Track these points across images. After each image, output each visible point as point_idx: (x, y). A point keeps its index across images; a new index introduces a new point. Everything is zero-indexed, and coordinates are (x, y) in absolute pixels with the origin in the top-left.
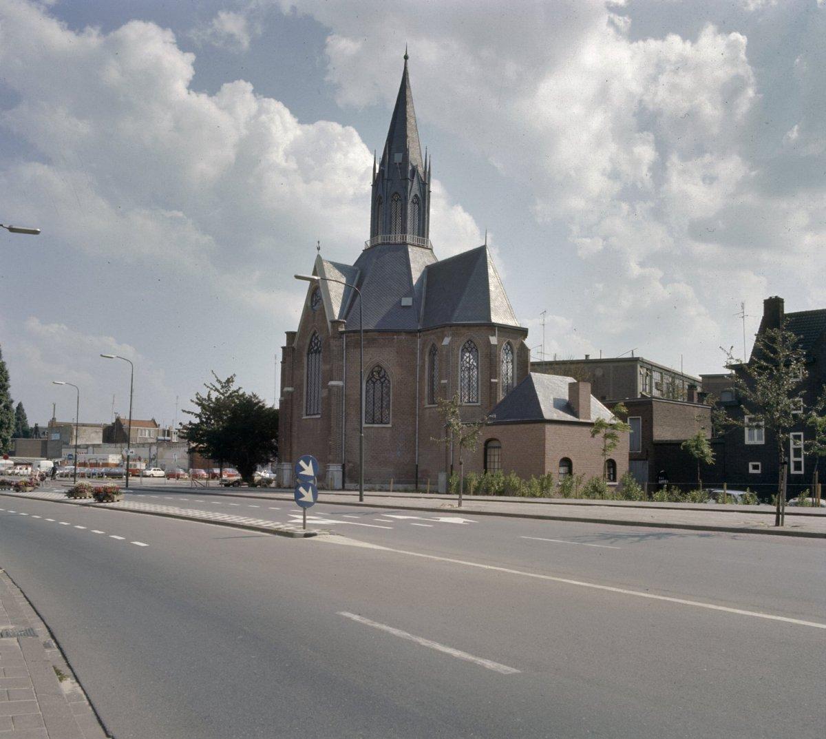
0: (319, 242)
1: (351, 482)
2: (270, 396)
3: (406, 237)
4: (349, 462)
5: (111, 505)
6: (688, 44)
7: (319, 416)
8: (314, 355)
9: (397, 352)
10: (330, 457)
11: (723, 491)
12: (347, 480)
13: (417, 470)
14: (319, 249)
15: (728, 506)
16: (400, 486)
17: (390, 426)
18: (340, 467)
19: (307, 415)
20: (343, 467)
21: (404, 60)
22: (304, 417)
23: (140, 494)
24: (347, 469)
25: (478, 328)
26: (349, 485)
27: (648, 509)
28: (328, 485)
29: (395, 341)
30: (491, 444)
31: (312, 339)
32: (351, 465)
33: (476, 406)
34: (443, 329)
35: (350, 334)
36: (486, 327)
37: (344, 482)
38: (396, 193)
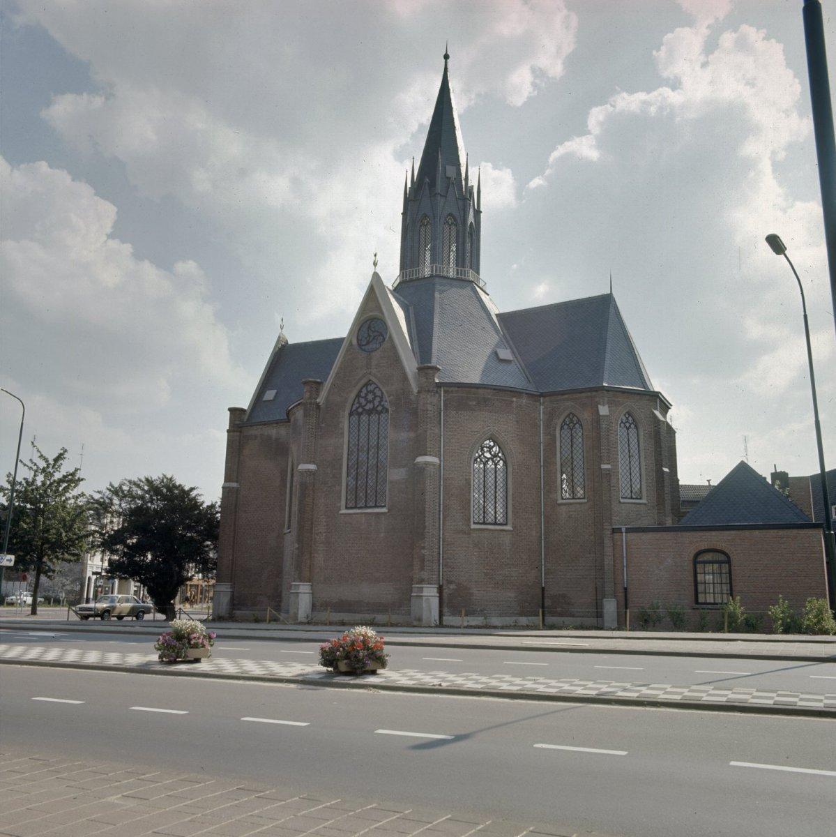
0: (375, 255)
1: (453, 614)
2: (208, 485)
3: (465, 271)
4: (450, 582)
5: (372, 680)
6: (149, 271)
7: (384, 510)
8: (364, 418)
9: (517, 422)
10: (425, 575)
11: (15, 609)
12: (445, 610)
13: (543, 595)
14: (375, 264)
15: (287, 627)
16: (523, 620)
17: (509, 528)
18: (436, 590)
19: (347, 508)
20: (440, 589)
21: (444, 60)
22: (344, 511)
23: (112, 640)
24: (446, 592)
25: (639, 397)
26: (450, 618)
27: (676, 641)
28: (420, 620)
29: (514, 405)
30: (700, 559)
31: (360, 391)
32: (452, 586)
33: (641, 504)
34: (594, 393)
35: (450, 389)
36: (648, 397)
37: (441, 615)
38: (450, 214)
